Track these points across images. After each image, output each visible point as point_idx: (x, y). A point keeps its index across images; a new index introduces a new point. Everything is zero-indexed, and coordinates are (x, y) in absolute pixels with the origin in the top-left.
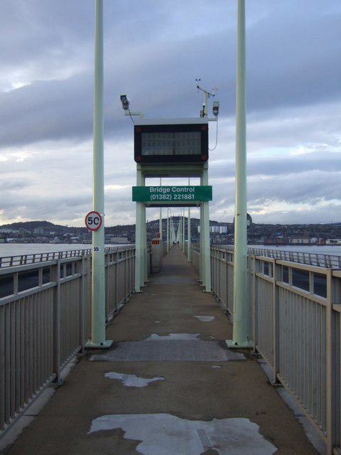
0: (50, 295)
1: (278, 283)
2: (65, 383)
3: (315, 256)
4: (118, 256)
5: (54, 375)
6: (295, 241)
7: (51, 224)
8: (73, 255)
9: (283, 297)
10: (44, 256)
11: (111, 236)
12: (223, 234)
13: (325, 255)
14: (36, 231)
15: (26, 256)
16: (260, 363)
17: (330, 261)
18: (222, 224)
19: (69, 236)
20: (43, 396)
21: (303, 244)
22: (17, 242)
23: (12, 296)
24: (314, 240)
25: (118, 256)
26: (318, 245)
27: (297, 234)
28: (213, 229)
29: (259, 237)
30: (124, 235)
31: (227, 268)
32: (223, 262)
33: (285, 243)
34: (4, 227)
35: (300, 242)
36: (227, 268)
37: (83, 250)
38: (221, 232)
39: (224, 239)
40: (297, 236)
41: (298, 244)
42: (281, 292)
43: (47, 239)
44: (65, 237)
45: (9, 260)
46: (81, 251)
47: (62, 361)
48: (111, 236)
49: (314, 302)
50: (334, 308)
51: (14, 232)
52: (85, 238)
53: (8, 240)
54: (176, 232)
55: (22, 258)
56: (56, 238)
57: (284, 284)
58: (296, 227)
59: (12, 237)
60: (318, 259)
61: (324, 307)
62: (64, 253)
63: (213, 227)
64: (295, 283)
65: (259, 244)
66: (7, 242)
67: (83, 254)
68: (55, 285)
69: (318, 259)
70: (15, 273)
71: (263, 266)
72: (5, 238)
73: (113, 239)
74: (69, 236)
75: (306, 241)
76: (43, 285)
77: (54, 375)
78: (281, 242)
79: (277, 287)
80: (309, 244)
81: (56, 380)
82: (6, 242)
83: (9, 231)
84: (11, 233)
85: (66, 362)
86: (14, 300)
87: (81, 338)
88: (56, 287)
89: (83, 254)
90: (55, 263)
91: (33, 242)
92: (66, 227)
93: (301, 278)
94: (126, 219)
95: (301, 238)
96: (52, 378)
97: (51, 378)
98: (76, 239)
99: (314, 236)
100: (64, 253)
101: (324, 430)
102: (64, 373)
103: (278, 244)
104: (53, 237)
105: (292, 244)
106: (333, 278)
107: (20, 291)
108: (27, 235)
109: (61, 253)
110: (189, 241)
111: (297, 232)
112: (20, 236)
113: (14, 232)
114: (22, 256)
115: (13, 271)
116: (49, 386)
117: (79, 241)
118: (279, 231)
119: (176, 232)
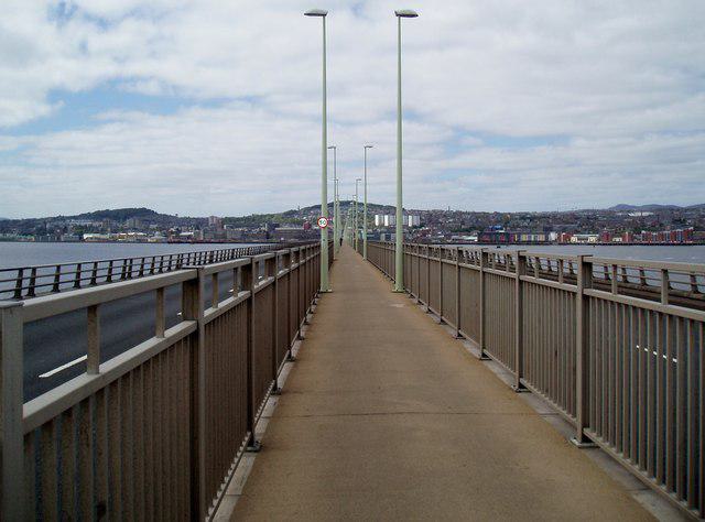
5: (249, 434)
8: (192, 260)
10: (165, 259)
12: (414, 227)
14: (128, 223)
15: (131, 260)
21: (537, 243)
38: (386, 224)
41: (529, 243)
44: (172, 233)
51: (96, 224)
53: (85, 236)
63: (386, 217)
67: (212, 256)
80: (547, 242)
82: (81, 239)
83: (88, 223)
86: (89, 392)
87: (274, 360)
89: (212, 256)
94: (185, 419)
95: (530, 233)
101: (575, 415)
114: (21, 270)
118: (498, 222)
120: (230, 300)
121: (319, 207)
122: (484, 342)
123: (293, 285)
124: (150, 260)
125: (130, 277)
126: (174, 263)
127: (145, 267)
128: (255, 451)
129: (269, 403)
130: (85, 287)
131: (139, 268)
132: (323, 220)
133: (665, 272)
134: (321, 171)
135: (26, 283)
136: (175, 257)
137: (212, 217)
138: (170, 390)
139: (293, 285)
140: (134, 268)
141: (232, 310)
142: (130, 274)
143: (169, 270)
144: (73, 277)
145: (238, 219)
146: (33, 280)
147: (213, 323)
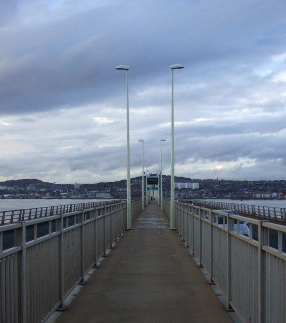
1: (264, 248)
2: (67, 309)
4: (97, 212)
5: (60, 302)
6: (258, 196)
7: (40, 182)
9: (268, 260)
11: (96, 193)
12: (196, 189)
13: (281, 209)
14: (29, 188)
15: (24, 210)
18: (195, 181)
19: (58, 193)
21: (265, 199)
22: (14, 198)
23: (13, 248)
24: (275, 194)
25: (97, 212)
26: (279, 199)
27: (262, 190)
28: (180, 185)
29: (227, 192)
30: (107, 191)
32: (205, 222)
33: (249, 198)
34: (2, 184)
35: (263, 197)
37: (84, 204)
38: (193, 188)
39: (195, 194)
40: (261, 191)
41: (261, 199)
42: (232, 238)
44: (55, 193)
46: (69, 206)
47: (98, 258)
48: (96, 193)
50: (263, 249)
51: (9, 189)
52: (72, 194)
53: (5, 196)
55: (21, 212)
56: (48, 194)
58: (261, 183)
59: (7, 194)
60: (275, 212)
61: (257, 248)
62: (55, 208)
65: (227, 198)
66: (4, 198)
67: (71, 208)
69: (275, 212)
72: (2, 194)
73: (97, 195)
74: (58, 193)
75: (268, 196)
76: (38, 239)
77: (60, 302)
78: (245, 196)
79: (263, 252)
80: (271, 199)
81: (82, 281)
82: (3, 198)
83: (4, 188)
84: (6, 190)
85: (47, 316)
87: (82, 270)
88: (20, 252)
89: (71, 208)
90: (59, 217)
91: (27, 197)
92: (54, 184)
96: (80, 280)
97: (56, 306)
98: (65, 195)
99: (274, 191)
100: (55, 208)
102: (86, 278)
103: (242, 199)
104: (45, 193)
105: (256, 199)
106: (262, 227)
107: (69, 226)
108: (21, 192)
109: (22, 212)
111: (262, 188)
112: (14, 193)
113: (9, 189)
115: (34, 223)
116: (57, 310)
117: (68, 197)
118: (245, 186)
122: (201, 256)
124: (40, 209)
126: (49, 211)
127: (6, 218)
128: (61, 311)
130: (43, 217)
131: (28, 215)
132: (34, 187)
133: (263, 207)
137: (77, 184)
138: (191, 202)
140: (25, 215)
142: (23, 218)
144: (10, 217)
145: (92, 185)
146: (23, 214)
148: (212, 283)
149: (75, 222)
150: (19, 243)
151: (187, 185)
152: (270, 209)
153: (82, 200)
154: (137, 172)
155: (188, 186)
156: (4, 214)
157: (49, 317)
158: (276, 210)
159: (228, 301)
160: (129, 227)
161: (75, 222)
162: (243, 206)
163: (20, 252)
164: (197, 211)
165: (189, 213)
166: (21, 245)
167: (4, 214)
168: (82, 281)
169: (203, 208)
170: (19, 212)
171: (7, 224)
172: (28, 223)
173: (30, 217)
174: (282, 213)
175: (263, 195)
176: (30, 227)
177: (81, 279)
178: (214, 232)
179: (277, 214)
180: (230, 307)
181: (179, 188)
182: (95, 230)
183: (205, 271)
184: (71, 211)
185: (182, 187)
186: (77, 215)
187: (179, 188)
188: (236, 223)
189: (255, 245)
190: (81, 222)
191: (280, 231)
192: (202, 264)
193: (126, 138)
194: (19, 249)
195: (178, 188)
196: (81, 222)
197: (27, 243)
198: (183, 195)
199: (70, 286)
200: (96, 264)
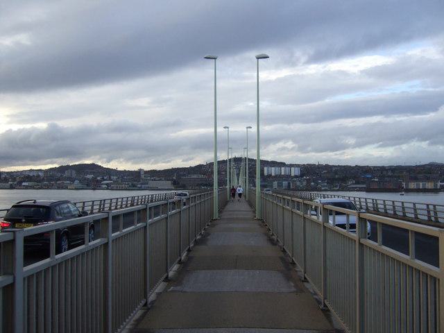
0: (141, 233)
1: (363, 241)
3: (412, 206)
6: (412, 185)
9: (367, 253)
10: (124, 199)
12: (296, 177)
13: (428, 205)
15: (104, 200)
16: (296, 271)
17: (436, 213)
20: (138, 313)
21: (425, 191)
23: (48, 260)
31: (305, 222)
32: (312, 221)
35: (421, 187)
36: (305, 222)
38: (293, 175)
40: (415, 179)
41: (418, 191)
43: (94, 185)
45: (91, 203)
49: (382, 254)
54: (238, 175)
57: (370, 243)
60: (366, 203)
64: (420, 255)
67: (152, 198)
68: (106, 241)
69: (385, 206)
70: (52, 231)
71: (296, 204)
75: (429, 185)
76: (124, 231)
79: (361, 245)
81: (167, 277)
87: (180, 250)
88: (106, 245)
89: (152, 198)
90: (144, 207)
93: (395, 237)
102: (171, 274)
104: (72, 180)
105: (408, 191)
107: (124, 229)
110: (258, 188)
115: (51, 229)
117: (109, 187)
119: (238, 175)
120: (133, 227)
121: (212, 164)
123: (206, 205)
125: (133, 206)
126: (129, 202)
127: (95, 207)
129: (160, 287)
134: (256, 154)
135: (119, 203)
136: (130, 199)
139: (206, 205)
141: (139, 229)
142: (103, 209)
143: (126, 206)
147: (171, 215)
148: (306, 280)
149: (136, 221)
150: (105, 235)
151: (283, 171)
152: (368, 200)
153: (139, 191)
154: (223, 156)
155: (285, 171)
156: (84, 204)
157: (134, 315)
158: (396, 204)
159: (322, 299)
160: (216, 216)
161: (136, 221)
162: (431, 207)
163: (106, 245)
164: (298, 206)
165: (278, 204)
166: (13, 274)
167: (84, 204)
168: (167, 277)
169: (278, 195)
170: (99, 203)
171: (96, 213)
172: (115, 212)
173: (116, 207)
174: (429, 212)
175: (421, 184)
176: (116, 217)
177: (165, 275)
178: (307, 224)
179: (362, 204)
180: (305, 278)
181: (273, 174)
182: (167, 228)
183: (311, 286)
184: (132, 205)
185: (277, 174)
186: (139, 211)
187: (273, 174)
188: (331, 214)
189: (424, 271)
190: (144, 220)
191: (412, 231)
192: (307, 277)
193: (213, 115)
194: (145, 224)
195: (271, 175)
196: (144, 220)
197: (113, 235)
198: (285, 183)
199: (154, 284)
200: (168, 276)
